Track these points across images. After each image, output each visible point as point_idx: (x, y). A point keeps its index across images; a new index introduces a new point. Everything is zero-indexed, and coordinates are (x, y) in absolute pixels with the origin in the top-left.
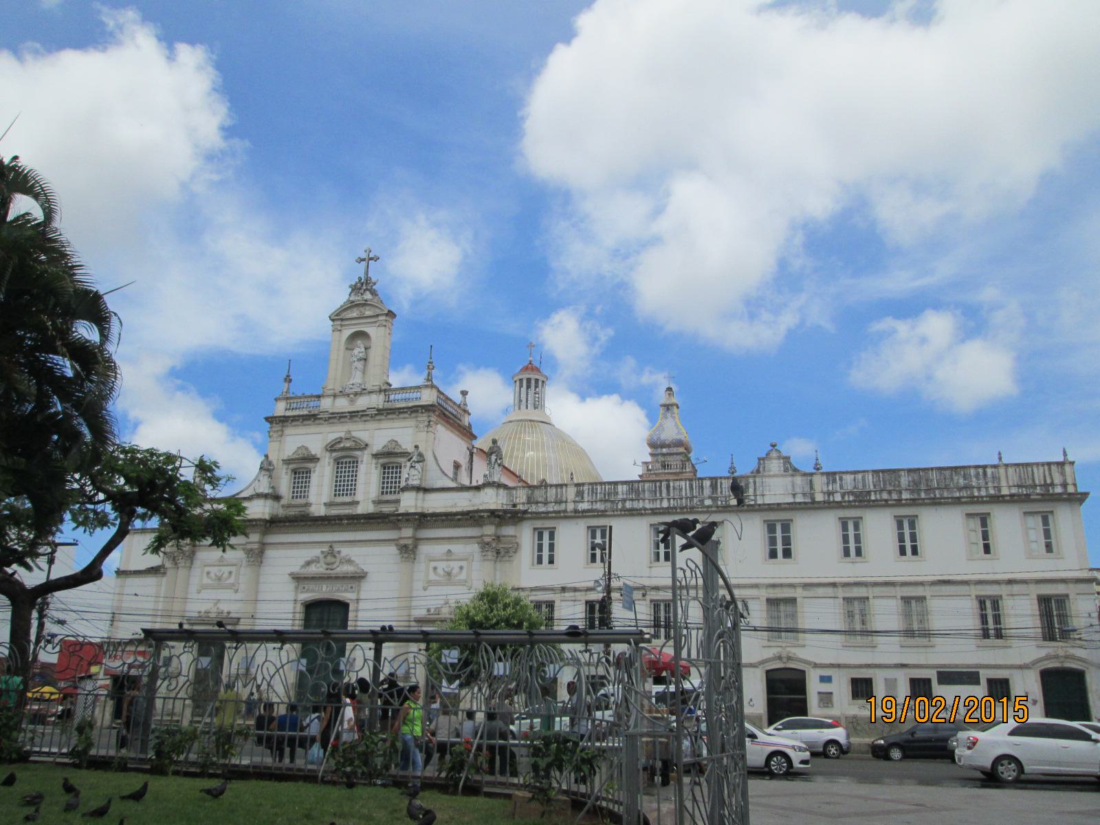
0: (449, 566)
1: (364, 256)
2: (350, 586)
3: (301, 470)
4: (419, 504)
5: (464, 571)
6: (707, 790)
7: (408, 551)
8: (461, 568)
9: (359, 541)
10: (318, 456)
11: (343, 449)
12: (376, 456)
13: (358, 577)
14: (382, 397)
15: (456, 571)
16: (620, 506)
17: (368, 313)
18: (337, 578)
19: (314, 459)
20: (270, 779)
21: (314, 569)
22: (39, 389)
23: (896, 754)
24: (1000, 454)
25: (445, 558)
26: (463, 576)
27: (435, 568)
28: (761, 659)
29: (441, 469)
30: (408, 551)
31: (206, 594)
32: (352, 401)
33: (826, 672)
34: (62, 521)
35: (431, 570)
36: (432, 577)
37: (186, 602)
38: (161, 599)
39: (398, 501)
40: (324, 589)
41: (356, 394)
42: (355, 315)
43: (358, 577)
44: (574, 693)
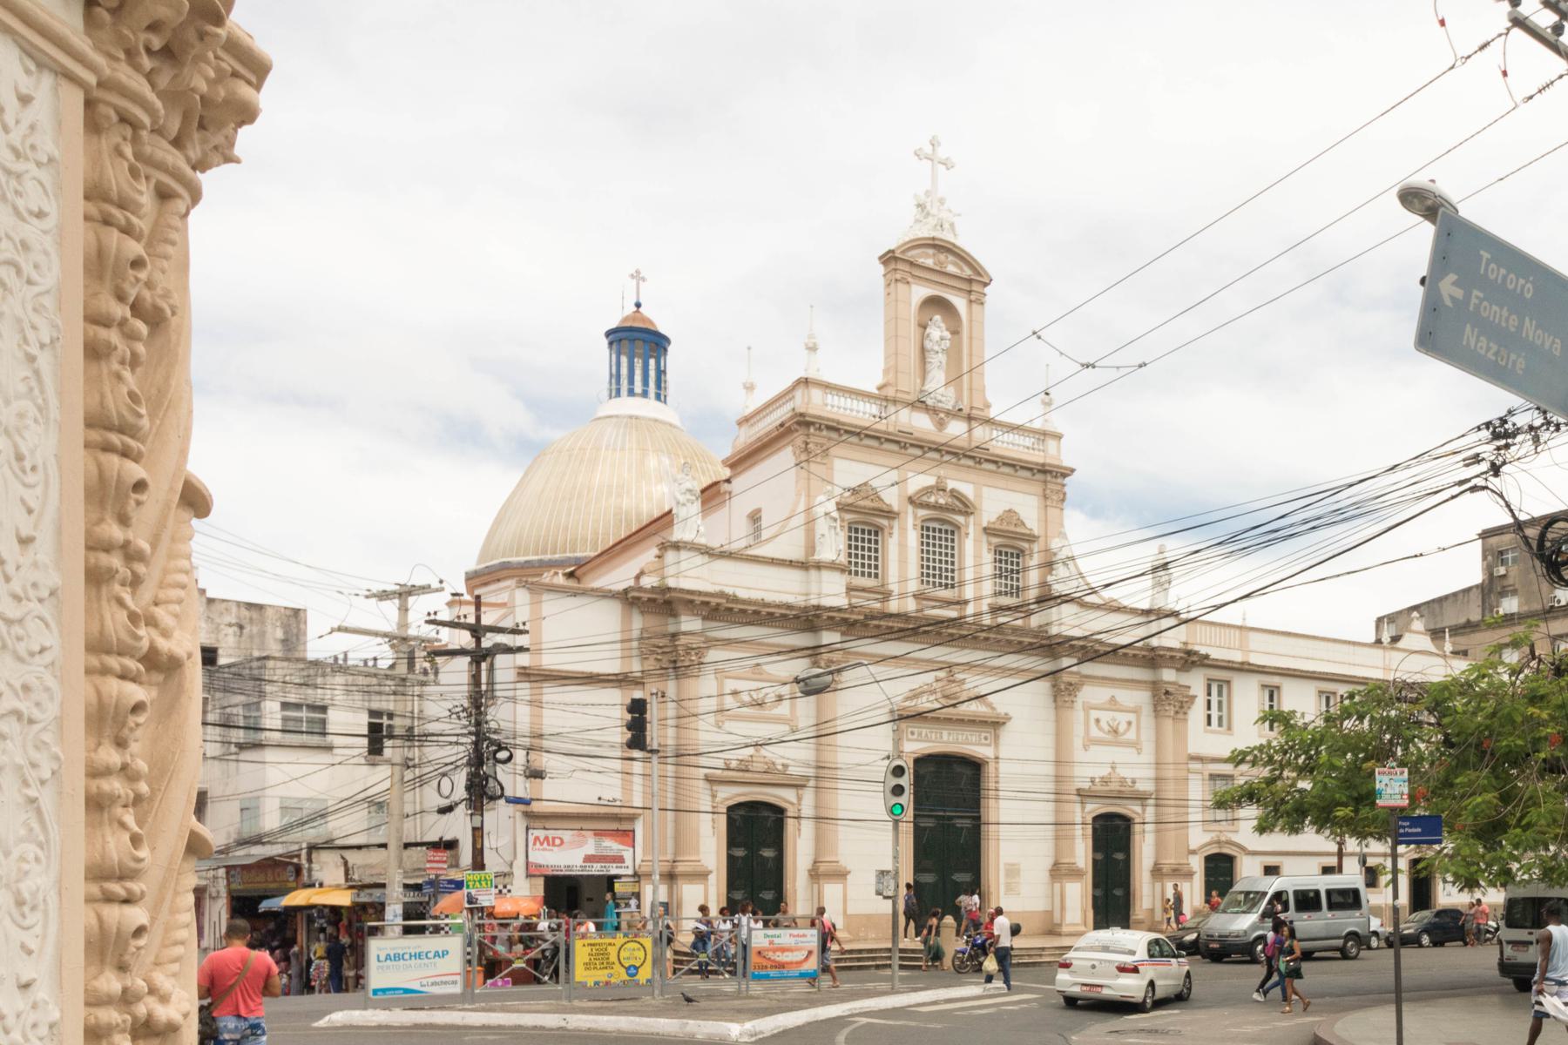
1: (942, 153)
2: (983, 735)
3: (1009, 550)
7: (1062, 692)
8: (1129, 723)
10: (896, 509)
11: (936, 507)
12: (988, 531)
13: (994, 724)
15: (1122, 728)
16: (26, 405)
17: (951, 269)
19: (890, 514)
21: (925, 703)
22: (1488, 344)
23: (1425, 940)
25: (1108, 706)
26: (1131, 735)
27: (1098, 721)
28: (517, 636)
34: (549, 571)
35: (1092, 722)
36: (1095, 732)
37: (817, 761)
38: (670, 722)
40: (945, 737)
42: (929, 262)
43: (994, 724)
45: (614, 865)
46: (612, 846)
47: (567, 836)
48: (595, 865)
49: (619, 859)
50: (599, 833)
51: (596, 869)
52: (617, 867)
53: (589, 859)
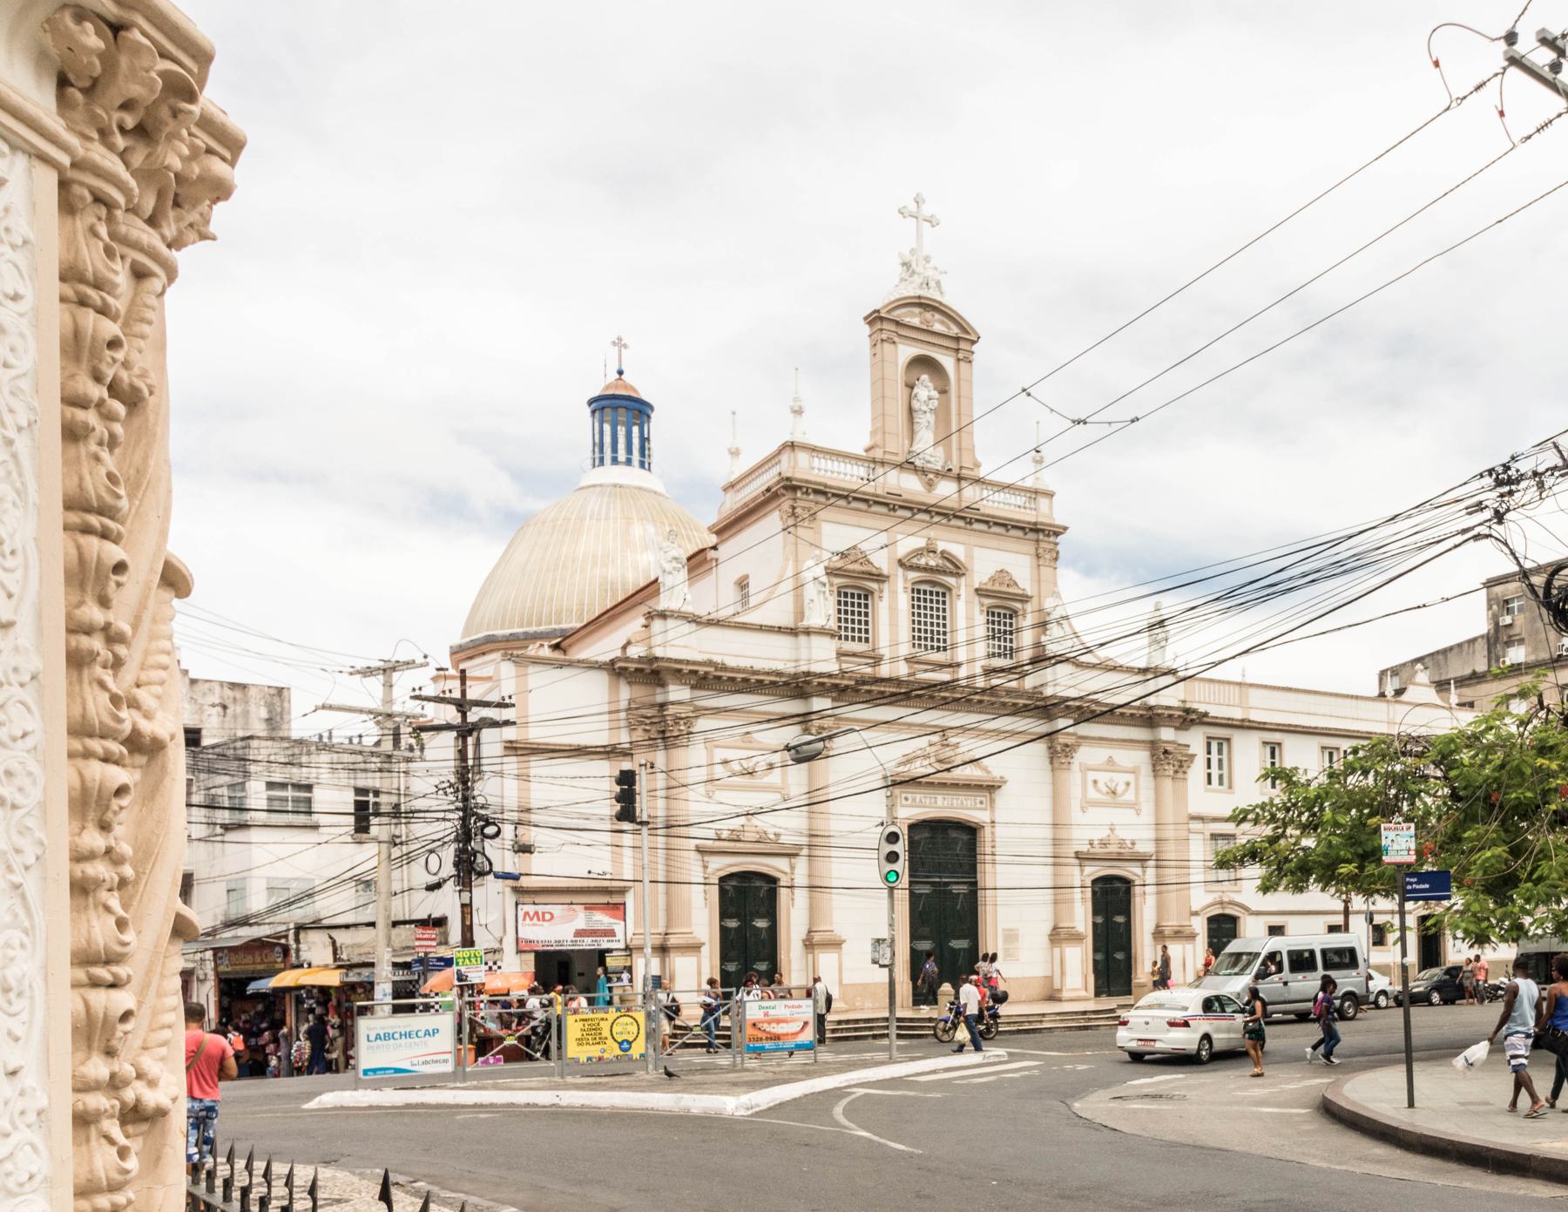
0: (1111, 780)
2: (979, 799)
4: (804, 655)
5: (1132, 786)
6: (880, 1077)
7: (1059, 753)
8: (1128, 784)
9: (1101, 739)
10: (885, 572)
11: (927, 569)
14: (862, 471)
15: (1120, 789)
17: (938, 327)
18: (955, 786)
19: (880, 578)
20: (417, 1104)
21: (918, 768)
23: (1436, 998)
24: (1244, 671)
26: (1130, 796)
27: (1095, 782)
29: (1226, 660)
30: (1059, 753)
31: (1095, 815)
32: (930, 485)
33: (1276, 921)
36: (1093, 794)
39: (841, 654)
40: (940, 802)
41: (937, 473)
42: (916, 321)
43: (990, 788)
44: (1489, 938)
45: (606, 939)
46: (602, 920)
47: (557, 910)
48: (586, 939)
49: (610, 933)
50: (589, 907)
51: (587, 943)
52: (608, 941)
53: (580, 933)
